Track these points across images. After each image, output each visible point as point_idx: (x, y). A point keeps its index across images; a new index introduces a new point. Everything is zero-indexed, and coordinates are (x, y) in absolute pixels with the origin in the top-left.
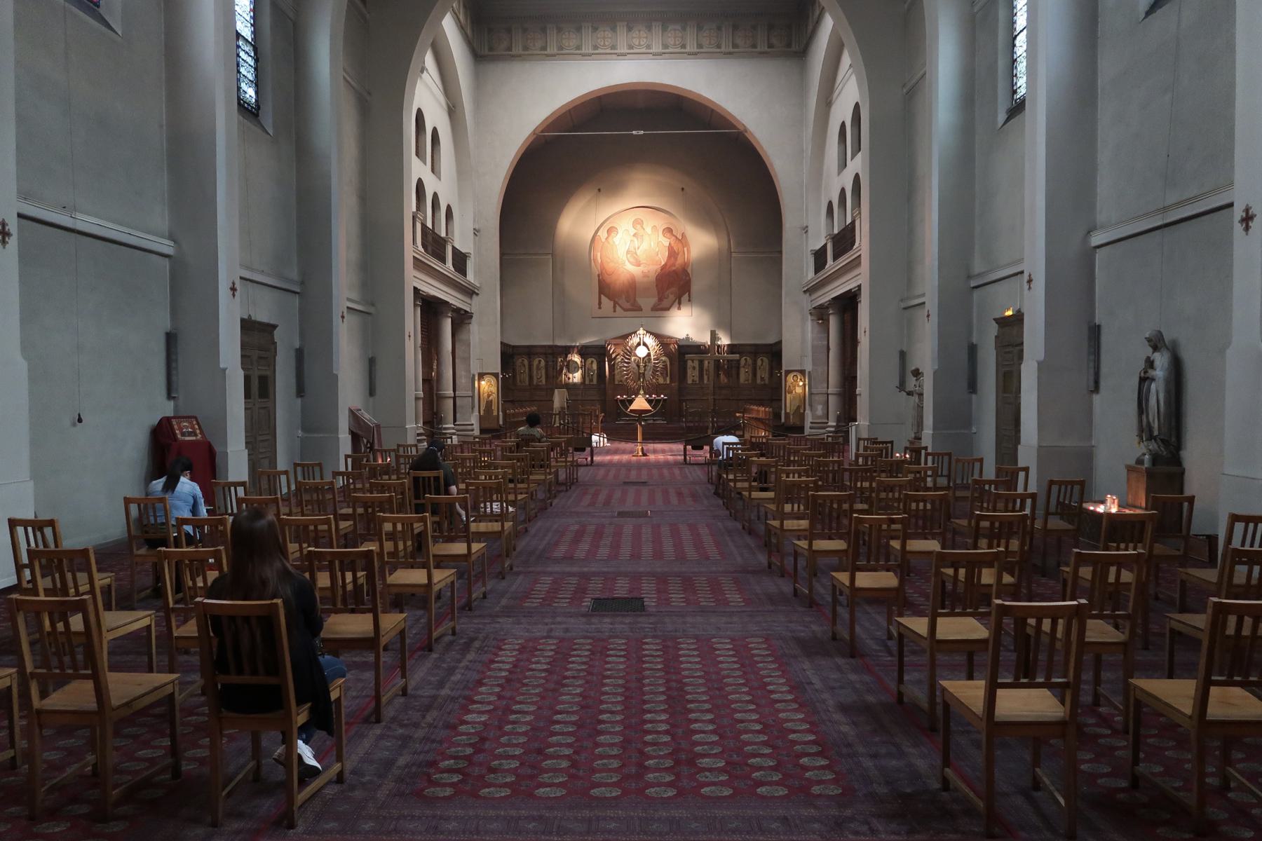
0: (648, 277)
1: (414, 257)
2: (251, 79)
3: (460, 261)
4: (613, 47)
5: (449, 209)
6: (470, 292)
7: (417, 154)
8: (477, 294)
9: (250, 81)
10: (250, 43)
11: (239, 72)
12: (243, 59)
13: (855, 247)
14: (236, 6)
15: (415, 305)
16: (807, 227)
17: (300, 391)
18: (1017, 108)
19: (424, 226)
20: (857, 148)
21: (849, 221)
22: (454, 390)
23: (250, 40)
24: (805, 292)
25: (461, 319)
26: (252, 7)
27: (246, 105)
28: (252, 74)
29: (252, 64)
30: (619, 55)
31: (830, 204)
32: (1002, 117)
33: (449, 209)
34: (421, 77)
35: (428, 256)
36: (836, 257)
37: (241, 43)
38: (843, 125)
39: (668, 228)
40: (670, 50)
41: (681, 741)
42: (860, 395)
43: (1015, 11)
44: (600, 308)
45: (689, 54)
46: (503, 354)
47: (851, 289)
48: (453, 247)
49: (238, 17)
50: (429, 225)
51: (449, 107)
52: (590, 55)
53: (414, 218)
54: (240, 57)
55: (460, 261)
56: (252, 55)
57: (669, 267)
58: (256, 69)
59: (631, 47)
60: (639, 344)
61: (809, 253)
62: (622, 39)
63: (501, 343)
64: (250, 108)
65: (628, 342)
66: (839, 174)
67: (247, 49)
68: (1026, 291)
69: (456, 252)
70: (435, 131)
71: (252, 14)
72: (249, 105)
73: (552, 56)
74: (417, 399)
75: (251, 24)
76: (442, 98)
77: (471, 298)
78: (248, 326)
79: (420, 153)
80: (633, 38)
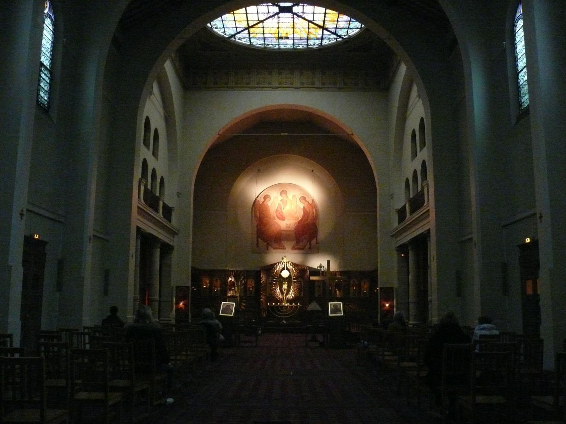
0: (290, 227)
1: (138, 206)
2: (47, 90)
3: (168, 211)
4: (270, 83)
5: (162, 179)
6: (173, 233)
7: (144, 144)
8: (178, 234)
9: (46, 91)
10: (49, 69)
11: (39, 85)
12: (43, 78)
13: (424, 205)
14: (42, 48)
15: (137, 237)
16: (393, 195)
17: (59, 286)
18: (524, 113)
19: (146, 187)
20: (423, 144)
21: (420, 189)
22: (160, 296)
23: (48, 67)
24: (392, 236)
25: (166, 249)
26: (52, 49)
27: (42, 105)
28: (48, 87)
29: (48, 81)
30: (273, 88)
31: (407, 180)
32: (513, 122)
33: (162, 179)
34: (149, 98)
35: (148, 207)
36: (412, 212)
37: (42, 69)
38: (414, 131)
39: (303, 197)
40: (305, 86)
41: (347, 279)
42: (431, 301)
43: (517, 59)
44: (257, 247)
45: (317, 88)
46: (193, 275)
47: (423, 233)
48: (164, 203)
49: (42, 54)
50: (149, 187)
51: (165, 116)
52: (255, 88)
53: (140, 182)
54: (41, 77)
55: (168, 211)
56: (49, 76)
57: (304, 222)
58: (50, 84)
59: (280, 83)
60: (283, 269)
61: (394, 211)
62: (275, 79)
63: (192, 267)
64: (44, 107)
65: (276, 267)
66: (412, 160)
67: (46, 72)
68: (539, 224)
69: (165, 206)
70: (156, 130)
71: (51, 53)
72: (43, 105)
73: (232, 88)
74: (135, 300)
75: (50, 59)
76: (161, 110)
77: (173, 237)
78: (28, 240)
79: (146, 143)
80: (282, 79)
